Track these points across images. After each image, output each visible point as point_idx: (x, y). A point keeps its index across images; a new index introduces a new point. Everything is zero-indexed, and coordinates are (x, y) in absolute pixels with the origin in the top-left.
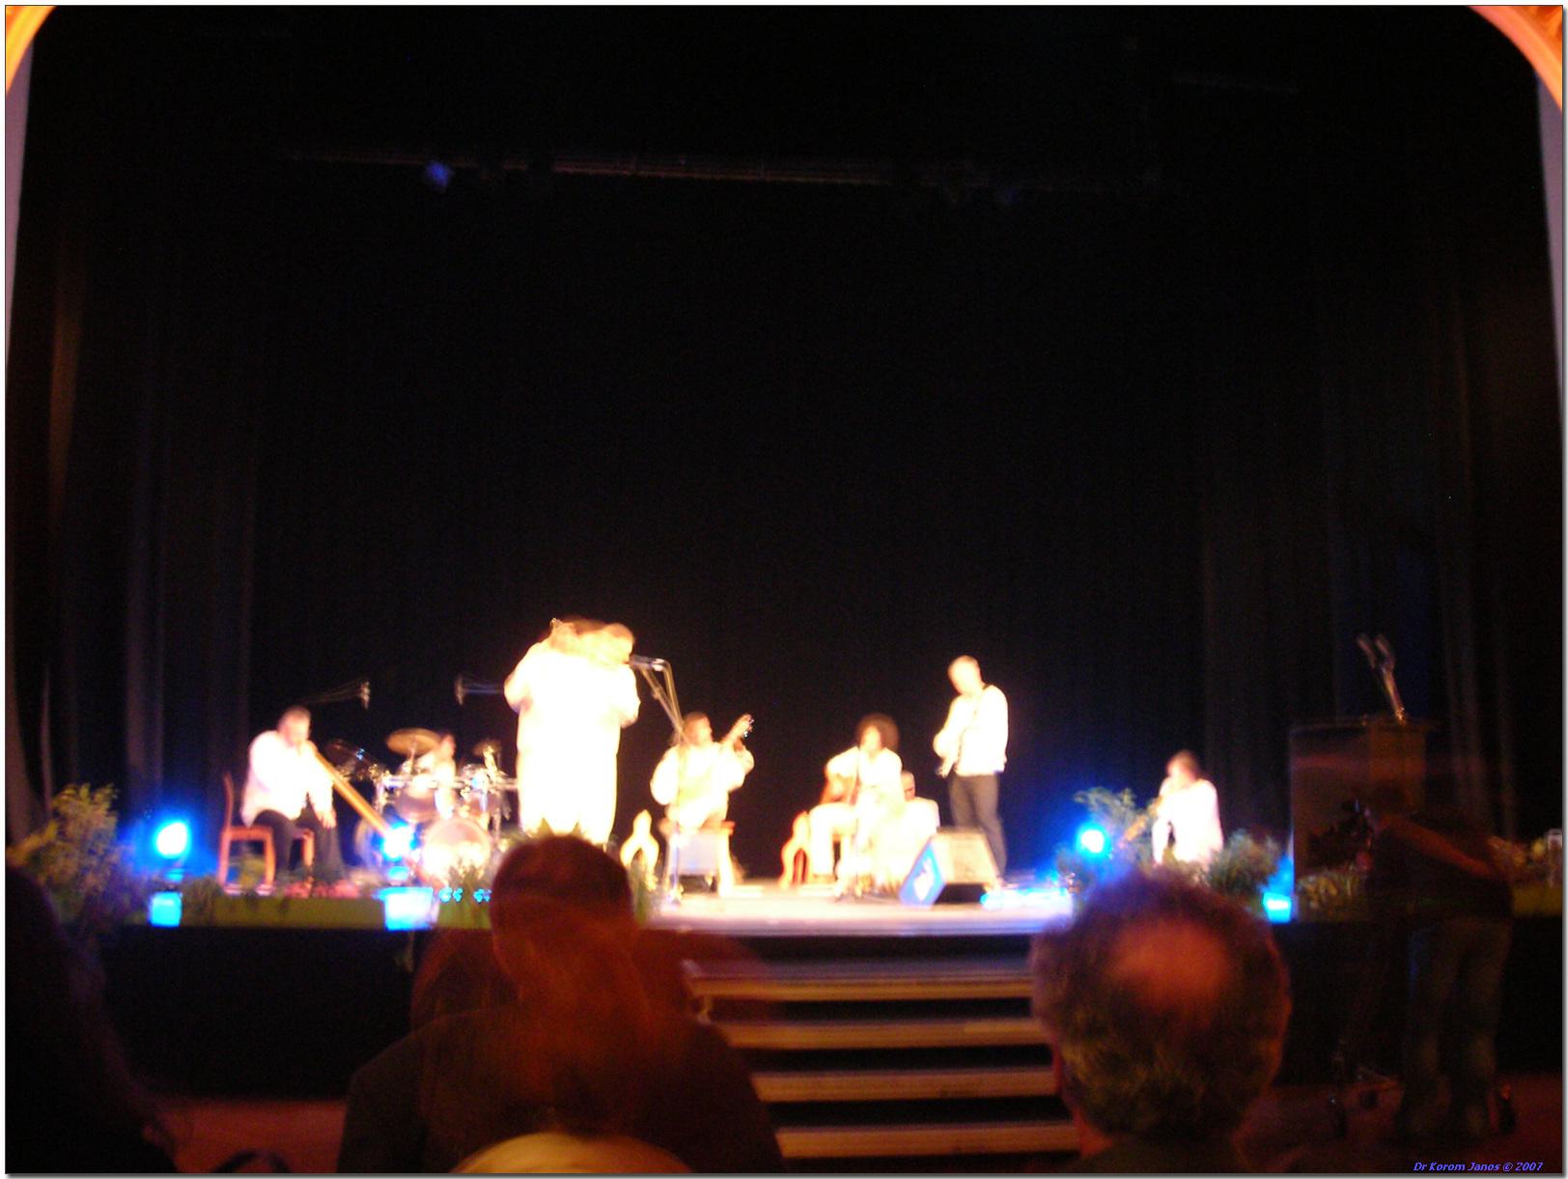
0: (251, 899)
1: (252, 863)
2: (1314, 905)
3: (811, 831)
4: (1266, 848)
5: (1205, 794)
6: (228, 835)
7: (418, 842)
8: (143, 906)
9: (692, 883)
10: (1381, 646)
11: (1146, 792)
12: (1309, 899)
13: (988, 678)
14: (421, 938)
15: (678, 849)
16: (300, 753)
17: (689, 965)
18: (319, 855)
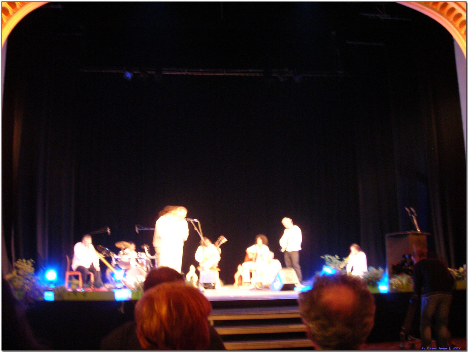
0: (75, 292)
2: (394, 287)
3: (243, 270)
6: (68, 274)
9: (208, 286)
10: (412, 209)
13: (294, 223)
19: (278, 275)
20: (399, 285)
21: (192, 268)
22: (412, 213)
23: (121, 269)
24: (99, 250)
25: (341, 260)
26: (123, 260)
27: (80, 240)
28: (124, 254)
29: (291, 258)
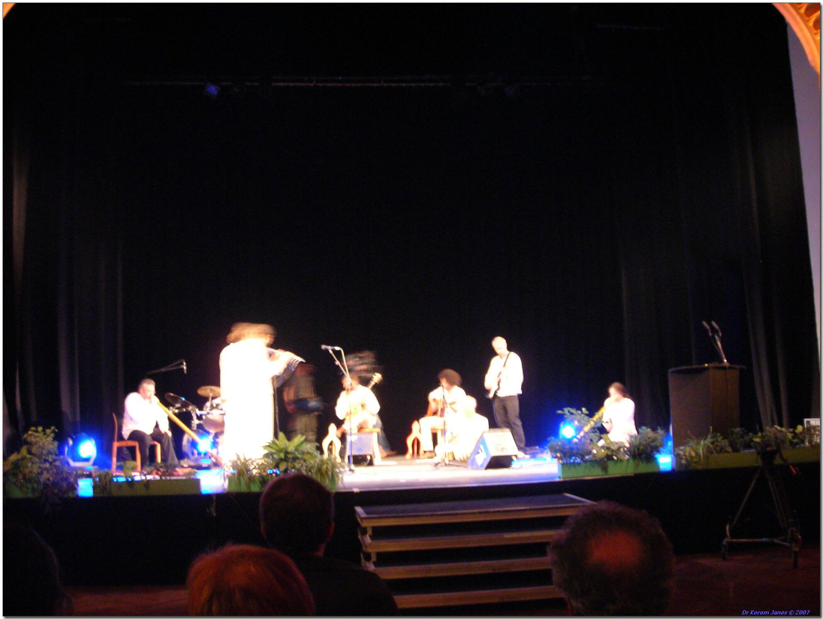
0: (131, 483)
1: (130, 463)
2: (684, 462)
3: (421, 429)
4: (658, 433)
5: (628, 406)
6: (116, 445)
7: (215, 444)
8: (73, 487)
9: (359, 460)
10: (714, 323)
11: (594, 403)
12: (681, 459)
13: (510, 348)
14: (220, 499)
15: (351, 442)
16: (151, 402)
17: (359, 509)
18: (164, 459)
19: (481, 441)
20: (691, 457)
21: (332, 428)
22: (714, 330)
23: (208, 433)
24: (166, 403)
25: (591, 415)
26: (210, 416)
27: (135, 388)
28: (212, 407)
29: (505, 409)
